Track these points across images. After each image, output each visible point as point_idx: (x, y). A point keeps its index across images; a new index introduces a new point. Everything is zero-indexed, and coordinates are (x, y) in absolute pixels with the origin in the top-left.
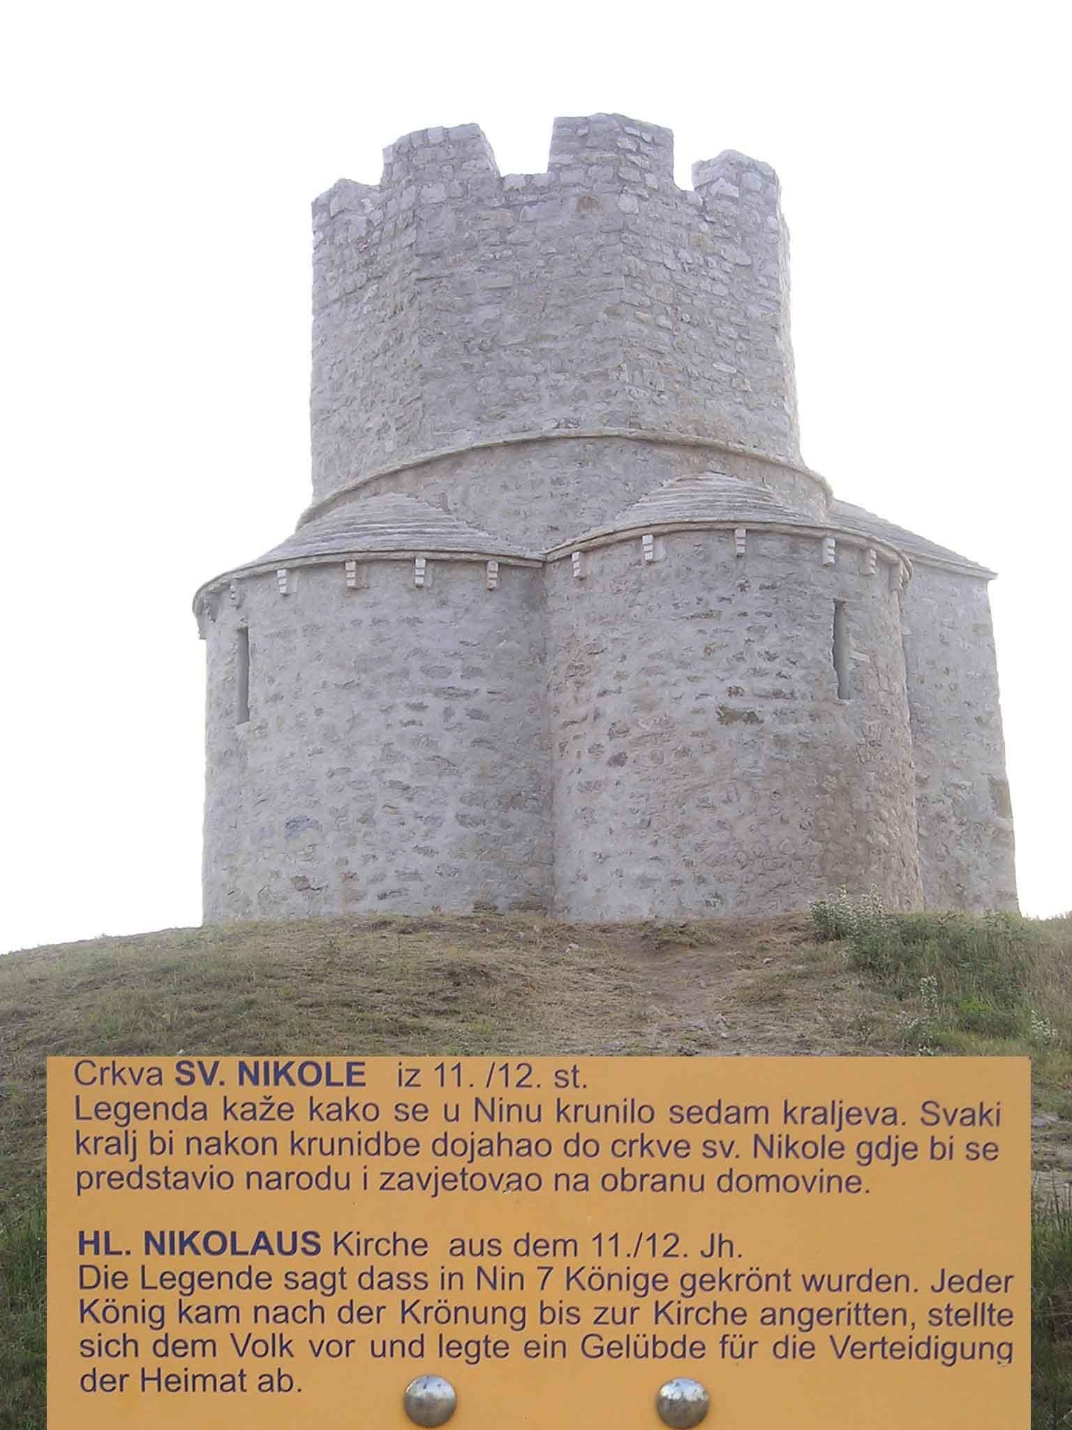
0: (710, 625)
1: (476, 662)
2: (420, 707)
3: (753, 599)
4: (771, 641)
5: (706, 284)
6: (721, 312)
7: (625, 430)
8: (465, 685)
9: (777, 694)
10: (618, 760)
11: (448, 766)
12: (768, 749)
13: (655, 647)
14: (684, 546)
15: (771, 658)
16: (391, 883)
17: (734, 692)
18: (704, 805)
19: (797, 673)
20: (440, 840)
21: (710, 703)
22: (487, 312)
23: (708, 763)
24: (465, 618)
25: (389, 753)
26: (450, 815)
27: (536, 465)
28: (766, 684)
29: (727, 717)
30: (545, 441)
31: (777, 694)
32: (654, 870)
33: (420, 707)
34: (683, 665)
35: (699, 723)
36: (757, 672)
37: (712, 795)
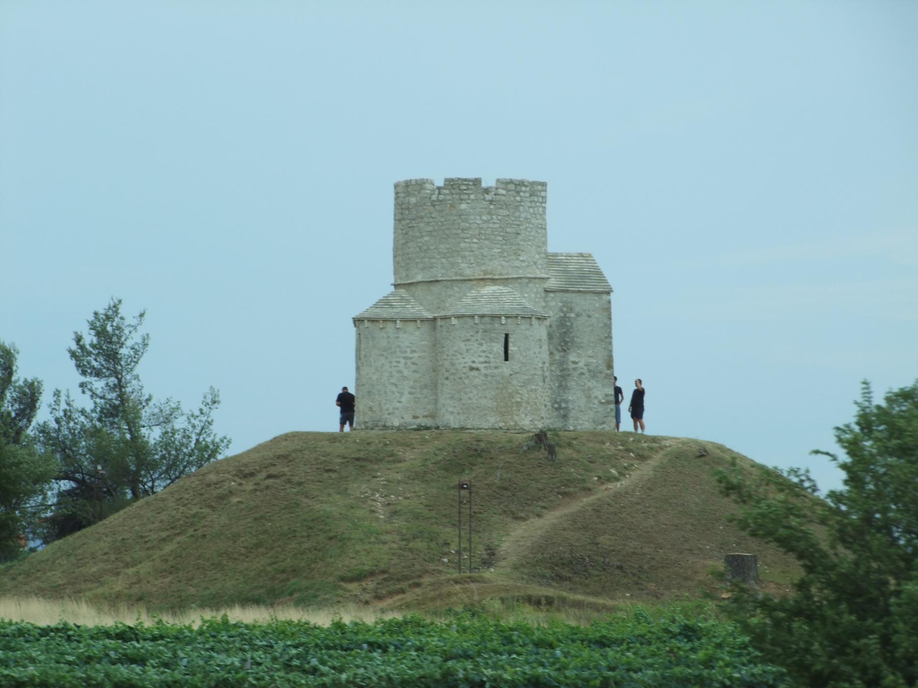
0: (468, 343)
1: (414, 348)
2: (398, 362)
3: (479, 336)
4: (484, 347)
5: (491, 225)
6: (496, 233)
7: (459, 278)
8: (412, 355)
9: (486, 362)
10: (447, 379)
11: (405, 378)
12: (482, 378)
13: (455, 349)
14: (461, 321)
15: (484, 352)
16: (391, 411)
17: (473, 362)
18: (466, 393)
19: (491, 356)
20: (403, 399)
21: (467, 365)
22: (426, 238)
23: (466, 381)
24: (426, 327)
25: (391, 376)
26: (406, 392)
27: (435, 288)
28: (482, 359)
29: (472, 369)
30: (437, 281)
31: (486, 362)
32: (454, 410)
33: (398, 362)
34: (461, 354)
35: (465, 370)
36: (480, 356)
37: (468, 390)
